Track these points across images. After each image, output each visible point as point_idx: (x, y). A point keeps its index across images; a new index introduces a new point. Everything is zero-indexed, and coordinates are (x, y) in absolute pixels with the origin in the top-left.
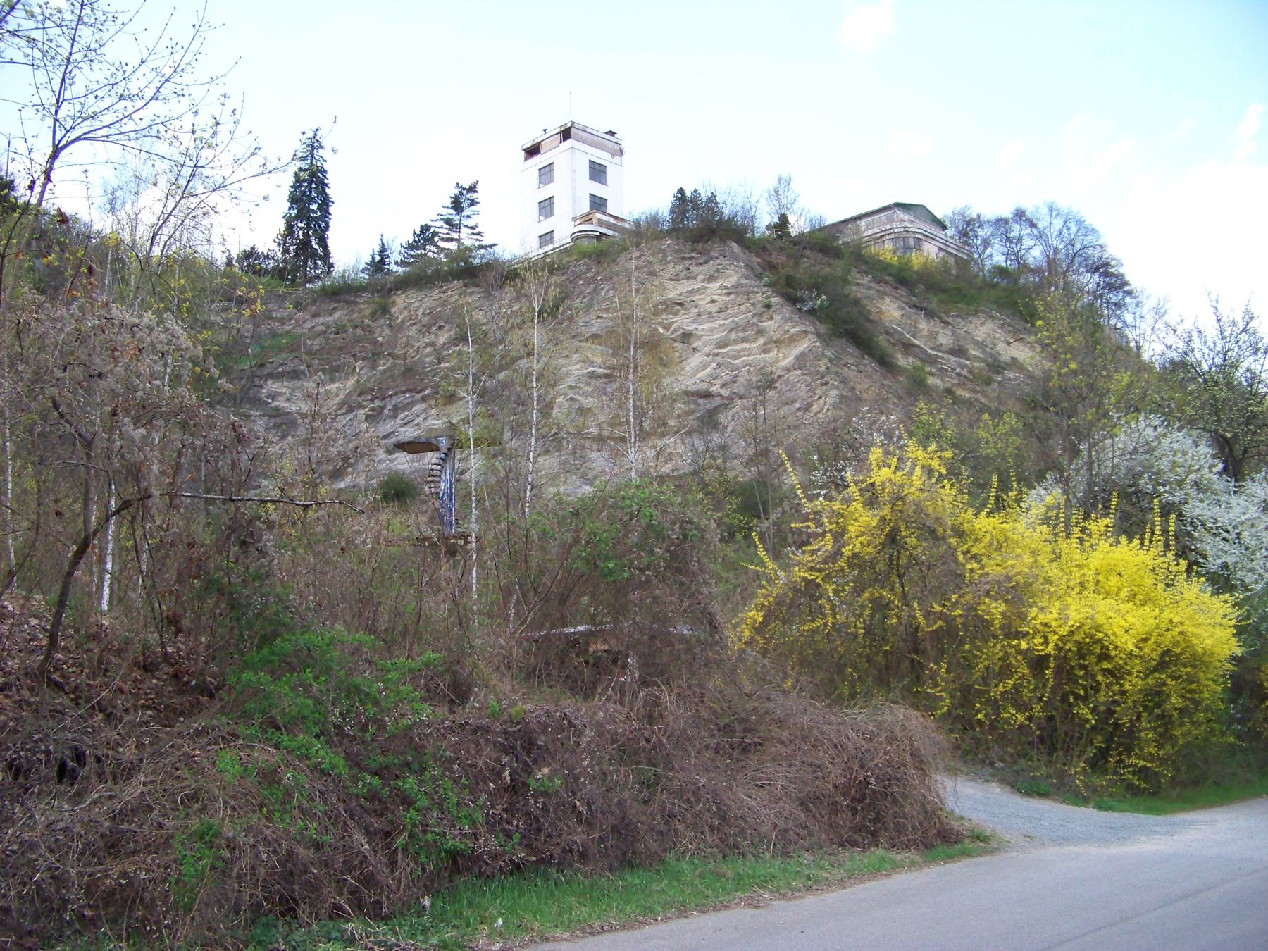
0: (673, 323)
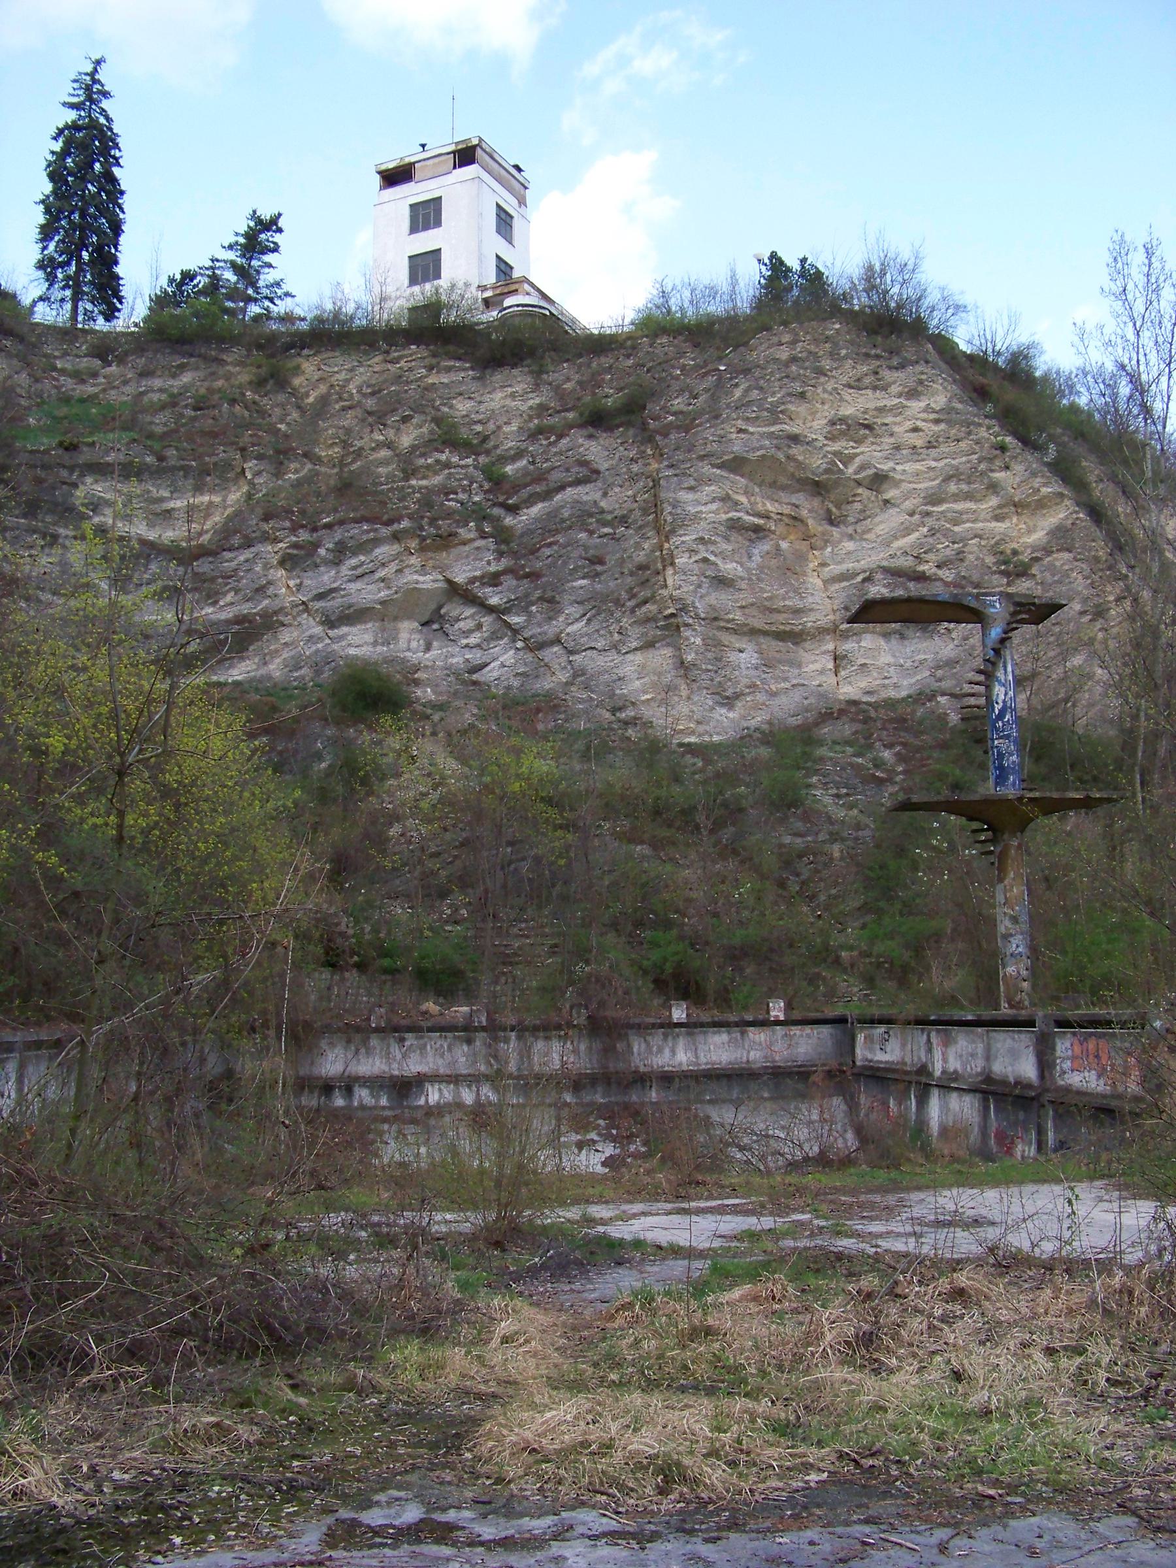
0: (857, 455)
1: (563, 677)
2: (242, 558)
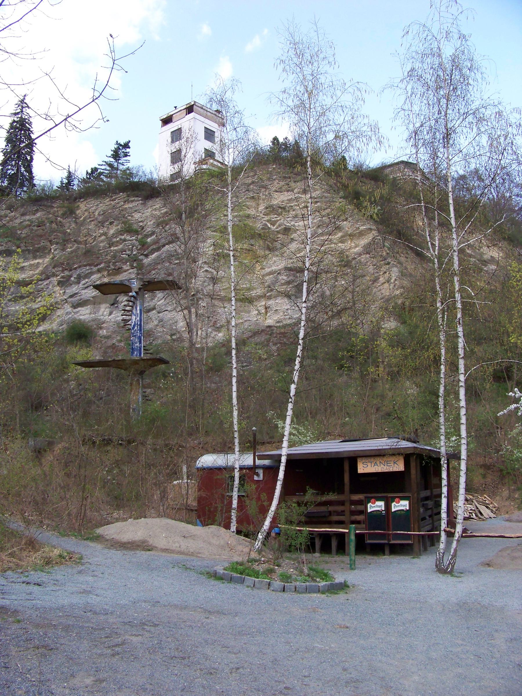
0: (278, 221)
1: (156, 323)
2: (45, 283)
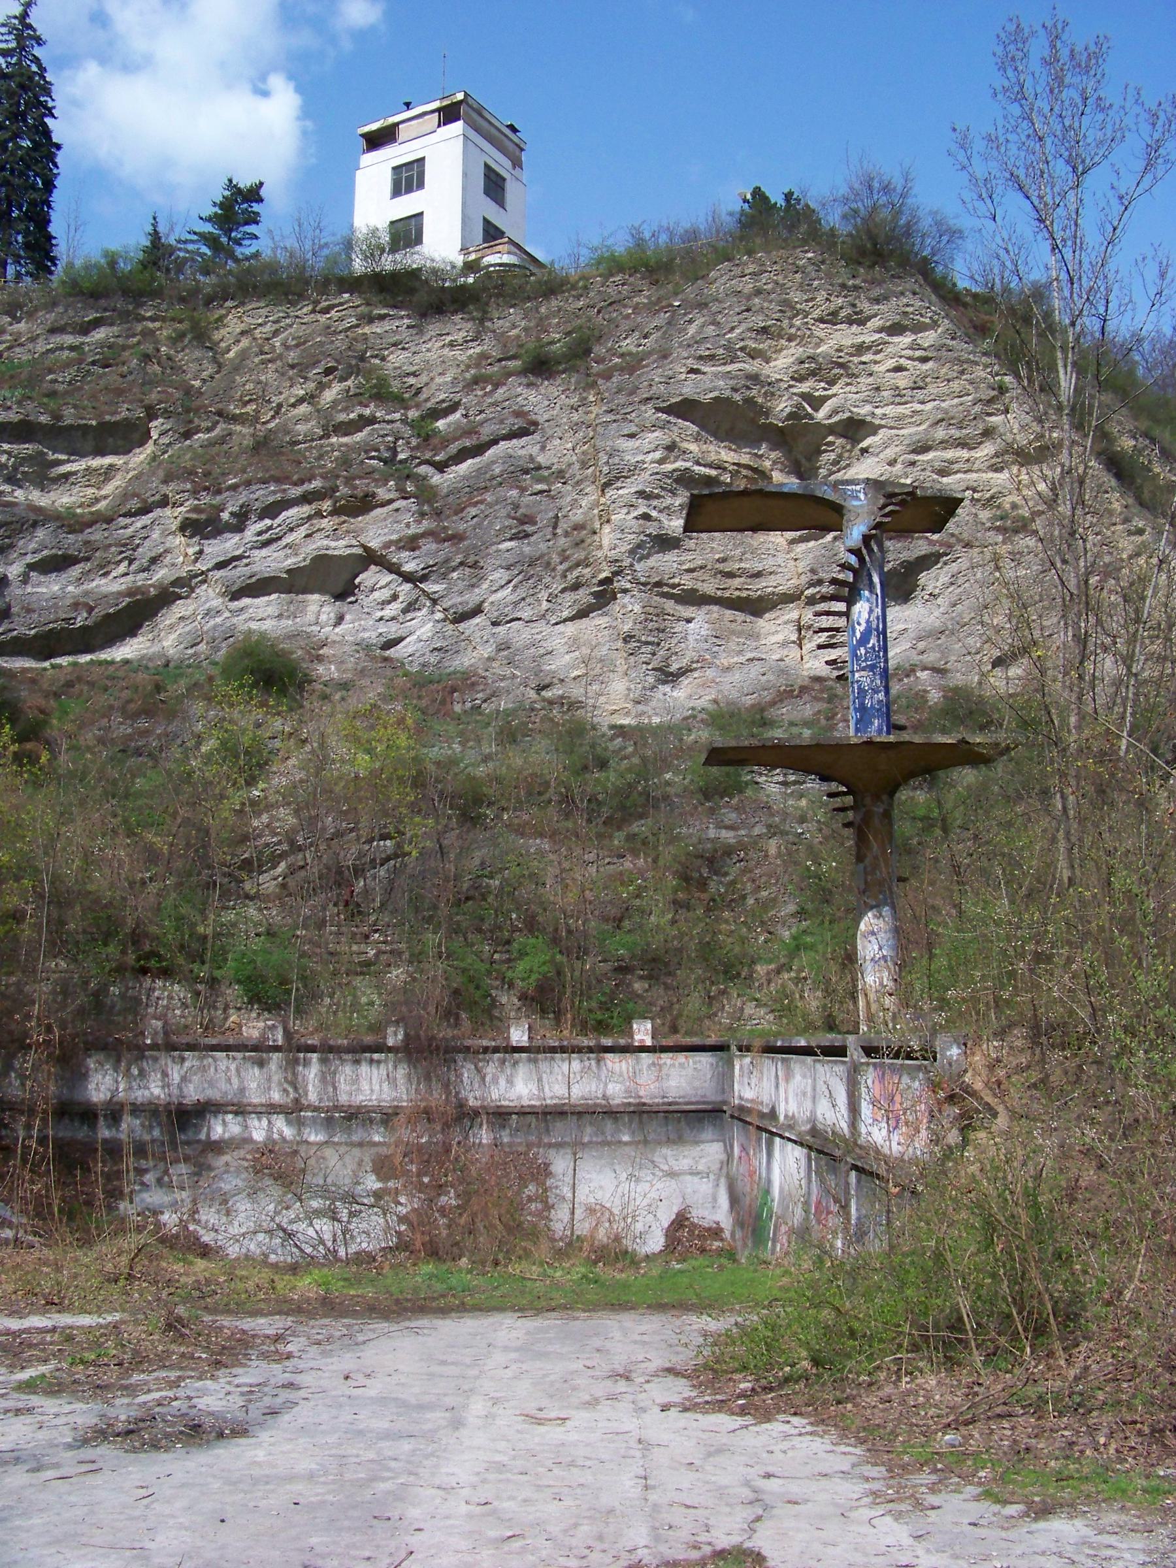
0: (829, 397)
1: (487, 651)
2: (139, 525)
